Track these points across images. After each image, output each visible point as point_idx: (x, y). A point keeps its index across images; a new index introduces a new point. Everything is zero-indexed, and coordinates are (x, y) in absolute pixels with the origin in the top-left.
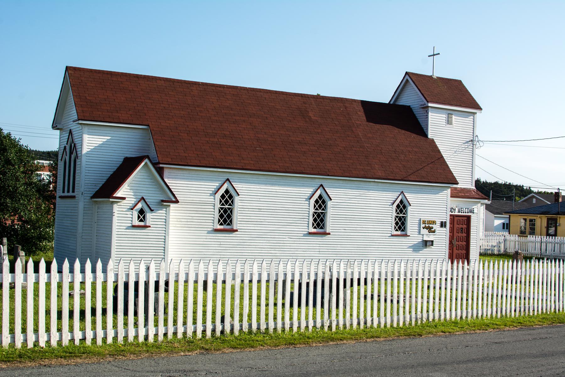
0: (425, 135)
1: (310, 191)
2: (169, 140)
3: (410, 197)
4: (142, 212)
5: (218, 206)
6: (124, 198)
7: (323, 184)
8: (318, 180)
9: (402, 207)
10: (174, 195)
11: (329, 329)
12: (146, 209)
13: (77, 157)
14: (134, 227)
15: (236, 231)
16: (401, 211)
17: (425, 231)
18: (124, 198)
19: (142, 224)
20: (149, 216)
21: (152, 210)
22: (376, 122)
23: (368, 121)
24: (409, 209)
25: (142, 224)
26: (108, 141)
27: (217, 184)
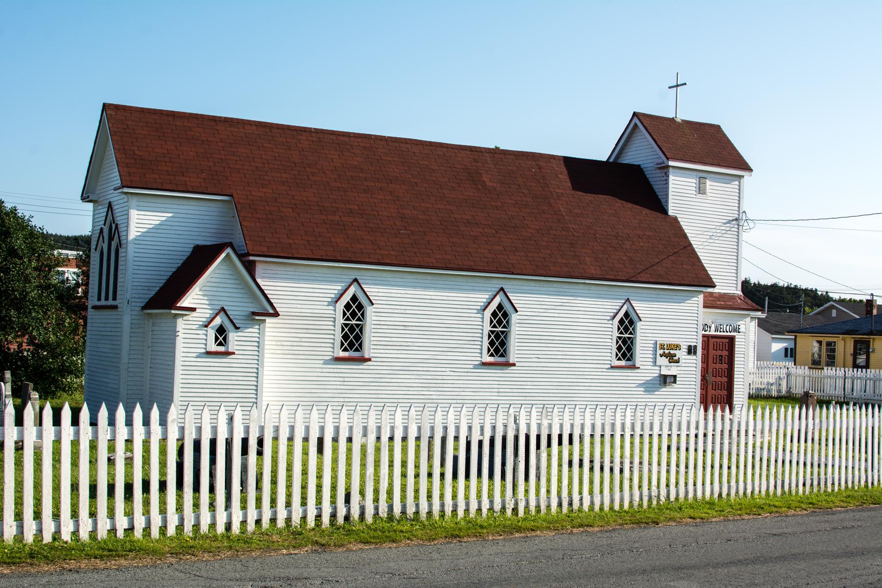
0: (664, 211)
1: (484, 297)
3: (640, 307)
4: (221, 330)
5: (341, 321)
6: (193, 310)
7: (504, 287)
8: (497, 281)
9: (627, 323)
10: (271, 304)
12: (228, 325)
13: (120, 244)
14: (209, 353)
15: (369, 360)
16: (626, 329)
17: (664, 361)
18: (193, 310)
20: (233, 336)
21: (237, 328)
22: (587, 191)
23: (575, 188)
24: (639, 325)
26: (168, 220)
27: (339, 287)
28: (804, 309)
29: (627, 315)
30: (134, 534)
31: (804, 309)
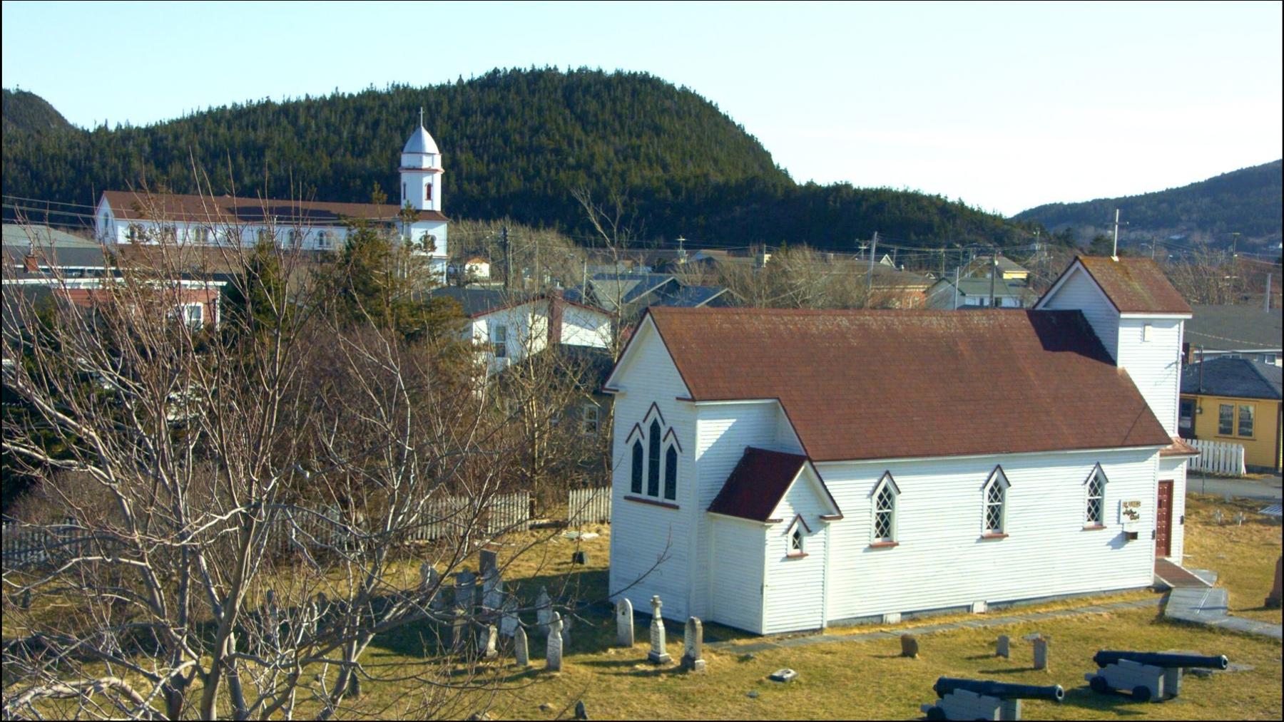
0: (1113, 362)
1: (985, 475)
2: (675, 436)
3: (1106, 468)
4: (797, 535)
5: (876, 510)
6: (780, 521)
7: (1002, 464)
8: (993, 459)
9: (1097, 485)
10: (837, 508)
11: (254, 252)
12: (803, 530)
13: (672, 454)
14: (789, 558)
15: (897, 544)
16: (1096, 492)
17: (1125, 518)
18: (780, 521)
19: (797, 551)
20: (807, 540)
21: (809, 531)
22: (1054, 350)
23: (1046, 347)
24: (1107, 487)
25: (797, 551)
26: (734, 425)
27: (876, 480)
28: (133, 369)
29: (1096, 478)
30: (615, 623)
31: (133, 369)
